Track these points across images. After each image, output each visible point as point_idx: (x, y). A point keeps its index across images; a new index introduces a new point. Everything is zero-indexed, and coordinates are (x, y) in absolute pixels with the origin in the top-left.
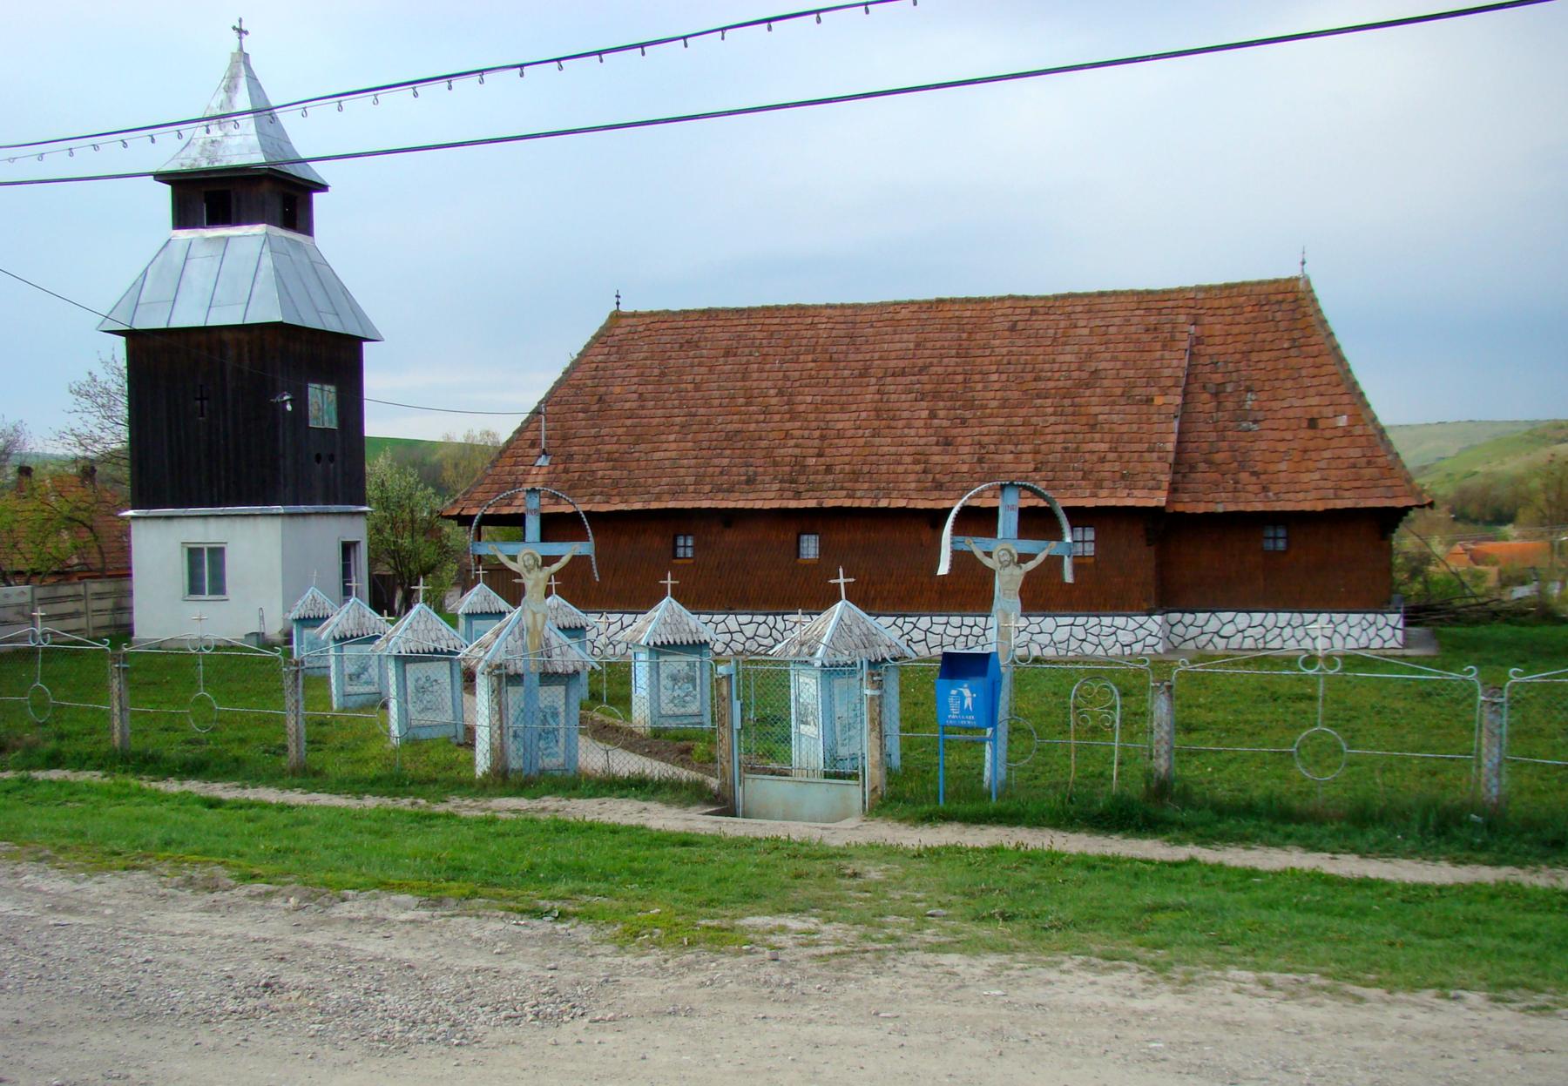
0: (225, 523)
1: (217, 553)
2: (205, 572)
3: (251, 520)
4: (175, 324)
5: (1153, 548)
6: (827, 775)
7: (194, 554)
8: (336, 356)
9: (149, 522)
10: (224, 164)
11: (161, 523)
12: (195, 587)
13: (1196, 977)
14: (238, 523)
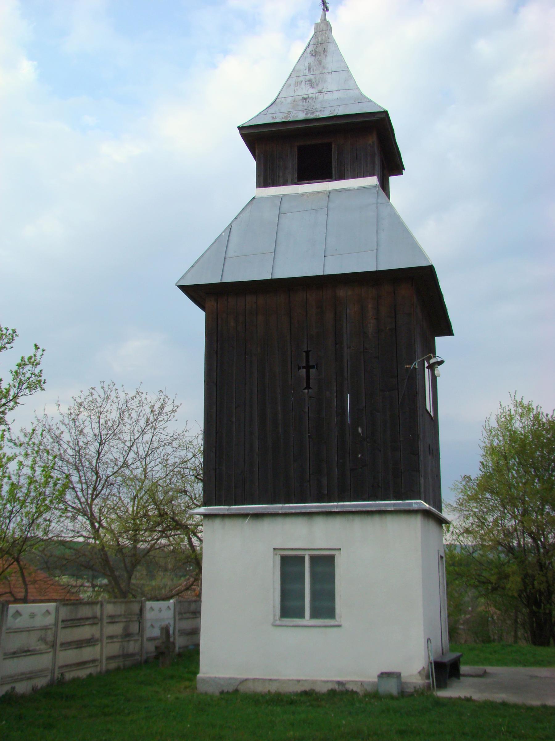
0: (337, 523)
1: (324, 564)
2: (307, 589)
3: (377, 519)
4: (278, 275)
5: (217, 693)
6: (340, 549)
7: (290, 564)
9: (229, 523)
10: (326, 114)
11: (247, 525)
12: (289, 608)
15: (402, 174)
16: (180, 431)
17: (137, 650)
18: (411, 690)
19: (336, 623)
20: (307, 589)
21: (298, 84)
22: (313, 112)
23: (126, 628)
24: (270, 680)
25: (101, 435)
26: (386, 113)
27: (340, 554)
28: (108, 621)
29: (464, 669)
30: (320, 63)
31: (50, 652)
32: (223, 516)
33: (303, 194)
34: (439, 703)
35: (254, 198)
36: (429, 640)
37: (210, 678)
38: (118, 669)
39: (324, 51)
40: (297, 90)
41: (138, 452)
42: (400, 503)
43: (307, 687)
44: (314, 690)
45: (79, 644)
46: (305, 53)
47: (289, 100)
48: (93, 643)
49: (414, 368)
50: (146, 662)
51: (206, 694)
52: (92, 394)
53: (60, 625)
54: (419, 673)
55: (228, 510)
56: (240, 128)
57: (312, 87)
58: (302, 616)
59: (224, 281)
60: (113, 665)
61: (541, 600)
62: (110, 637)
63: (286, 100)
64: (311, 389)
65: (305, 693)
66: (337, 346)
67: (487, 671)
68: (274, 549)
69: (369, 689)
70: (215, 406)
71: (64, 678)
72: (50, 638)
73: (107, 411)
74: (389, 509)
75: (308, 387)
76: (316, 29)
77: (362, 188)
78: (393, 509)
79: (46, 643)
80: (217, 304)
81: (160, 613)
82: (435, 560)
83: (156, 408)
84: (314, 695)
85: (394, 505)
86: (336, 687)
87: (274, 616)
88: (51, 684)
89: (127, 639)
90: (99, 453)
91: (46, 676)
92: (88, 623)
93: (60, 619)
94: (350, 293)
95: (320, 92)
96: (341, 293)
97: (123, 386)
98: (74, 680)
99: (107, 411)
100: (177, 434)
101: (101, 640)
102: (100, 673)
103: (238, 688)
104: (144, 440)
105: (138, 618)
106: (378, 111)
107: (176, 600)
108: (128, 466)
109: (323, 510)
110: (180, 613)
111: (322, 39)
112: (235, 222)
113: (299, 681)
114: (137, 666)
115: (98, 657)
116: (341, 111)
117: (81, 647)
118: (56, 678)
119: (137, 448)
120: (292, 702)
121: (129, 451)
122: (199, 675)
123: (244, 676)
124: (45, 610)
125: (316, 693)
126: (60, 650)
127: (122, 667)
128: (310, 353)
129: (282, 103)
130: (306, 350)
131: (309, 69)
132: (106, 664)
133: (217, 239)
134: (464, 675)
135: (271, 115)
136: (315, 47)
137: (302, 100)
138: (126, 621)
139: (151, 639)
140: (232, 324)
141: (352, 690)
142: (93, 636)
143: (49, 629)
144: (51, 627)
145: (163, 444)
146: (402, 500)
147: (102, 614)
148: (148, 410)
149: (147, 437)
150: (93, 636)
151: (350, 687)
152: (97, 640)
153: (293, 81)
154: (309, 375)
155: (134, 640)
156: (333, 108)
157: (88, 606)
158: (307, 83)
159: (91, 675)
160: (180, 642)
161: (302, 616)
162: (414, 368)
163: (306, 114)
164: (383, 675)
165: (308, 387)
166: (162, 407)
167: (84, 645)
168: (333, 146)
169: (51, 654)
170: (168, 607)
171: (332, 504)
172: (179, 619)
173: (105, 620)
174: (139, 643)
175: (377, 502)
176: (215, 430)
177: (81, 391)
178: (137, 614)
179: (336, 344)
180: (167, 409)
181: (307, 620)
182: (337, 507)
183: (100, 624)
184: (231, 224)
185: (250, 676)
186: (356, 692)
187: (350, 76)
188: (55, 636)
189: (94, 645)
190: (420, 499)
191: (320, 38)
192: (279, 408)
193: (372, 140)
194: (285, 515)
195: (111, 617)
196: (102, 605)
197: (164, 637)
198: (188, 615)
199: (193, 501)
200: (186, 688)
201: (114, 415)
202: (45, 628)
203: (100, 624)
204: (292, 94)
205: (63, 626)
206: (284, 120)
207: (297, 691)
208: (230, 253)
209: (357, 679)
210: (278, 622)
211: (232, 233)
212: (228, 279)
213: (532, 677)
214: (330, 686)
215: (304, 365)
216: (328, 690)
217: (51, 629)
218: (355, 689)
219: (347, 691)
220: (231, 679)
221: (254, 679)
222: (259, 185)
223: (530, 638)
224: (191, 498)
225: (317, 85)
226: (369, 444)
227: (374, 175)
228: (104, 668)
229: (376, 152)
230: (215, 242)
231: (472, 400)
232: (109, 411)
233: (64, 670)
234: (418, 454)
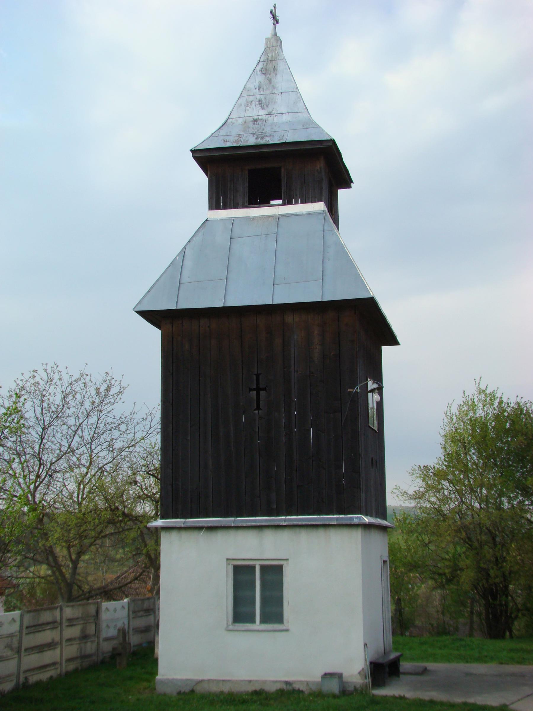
0: (285, 535)
1: (273, 573)
2: (257, 594)
3: (321, 532)
5: (175, 694)
6: (288, 559)
7: (242, 573)
8: (359, 329)
9: (185, 535)
10: (275, 140)
12: (241, 614)
16: (127, 414)
18: (352, 688)
19: (284, 628)
20: (257, 594)
21: (249, 104)
22: (263, 137)
23: (83, 630)
24: (224, 681)
25: (44, 420)
26: (333, 141)
27: (288, 564)
28: (67, 624)
29: (405, 665)
30: (270, 82)
32: (180, 529)
33: (254, 218)
34: (375, 701)
35: (206, 220)
36: (365, 645)
38: (76, 671)
39: (274, 69)
40: (248, 110)
41: (82, 436)
42: (343, 517)
43: (257, 687)
44: (264, 690)
45: (41, 648)
46: (255, 71)
47: (240, 121)
49: (356, 392)
50: (103, 662)
51: (165, 694)
52: (34, 377)
53: (25, 631)
54: (359, 673)
55: (184, 523)
56: (193, 151)
58: (253, 621)
59: (179, 307)
60: (72, 667)
62: (69, 640)
63: (237, 121)
64: (261, 410)
65: (257, 693)
66: (285, 370)
68: (227, 559)
69: (314, 688)
70: (171, 425)
72: (15, 644)
73: (50, 394)
74: (333, 523)
75: (258, 408)
77: (310, 214)
78: (336, 523)
79: (12, 649)
81: (115, 613)
82: (378, 564)
83: (102, 390)
85: (337, 519)
87: (228, 621)
88: (16, 689)
89: (84, 641)
90: (42, 438)
91: (13, 680)
92: (49, 627)
93: (25, 625)
95: (270, 114)
97: (66, 368)
98: (38, 683)
99: (50, 394)
100: (124, 417)
101: (61, 643)
103: (195, 689)
104: (90, 423)
105: (95, 619)
106: (325, 139)
107: (130, 599)
108: (73, 451)
109: (272, 523)
110: (134, 612)
111: (272, 57)
112: (188, 246)
113: (250, 681)
114: (94, 667)
115: (58, 660)
116: (291, 137)
118: (21, 682)
119: (82, 431)
120: (244, 702)
121: (74, 435)
122: (158, 677)
123: (201, 678)
125: (266, 693)
126: (25, 655)
127: (80, 668)
128: (260, 376)
130: (256, 373)
131: (260, 88)
132: (66, 666)
133: (171, 263)
134: (404, 673)
135: (222, 138)
136: (265, 64)
137: (253, 121)
138: (83, 624)
139: (107, 639)
141: (299, 689)
142: (53, 640)
143: (14, 636)
145: (109, 428)
147: (61, 618)
148: (93, 393)
149: (93, 420)
150: (53, 640)
151: (297, 686)
152: (57, 644)
153: (243, 100)
154: (259, 396)
155: (91, 641)
157: (48, 612)
158: (257, 103)
159: (51, 677)
160: (134, 640)
161: (253, 621)
162: (356, 392)
163: (256, 139)
164: (327, 676)
165: (258, 408)
166: (108, 389)
167: (45, 649)
168: (283, 170)
169: (16, 660)
171: (281, 517)
172: (134, 618)
173: (65, 623)
174: (95, 644)
175: (322, 516)
177: (23, 374)
178: (94, 616)
179: (284, 368)
180: (114, 390)
181: (258, 625)
182: (285, 520)
184: (184, 248)
185: (206, 677)
186: (302, 692)
187: (300, 97)
188: (20, 642)
189: (55, 648)
190: (361, 514)
191: (270, 55)
193: (320, 165)
194: (237, 528)
195: (69, 620)
196: (61, 610)
197: (121, 638)
198: (141, 613)
199: (143, 492)
200: (145, 689)
201: (58, 400)
202: (11, 636)
203: (59, 628)
204: (242, 115)
206: (235, 145)
207: (248, 691)
208: (185, 279)
210: (231, 627)
211: (186, 257)
213: (468, 674)
214: (278, 686)
216: (277, 690)
217: (16, 636)
218: (301, 689)
220: (187, 680)
222: (211, 208)
224: (141, 488)
225: (267, 106)
227: (321, 201)
228: (64, 671)
229: (324, 177)
230: (170, 266)
231: (418, 406)
232: (52, 394)
233: (28, 674)
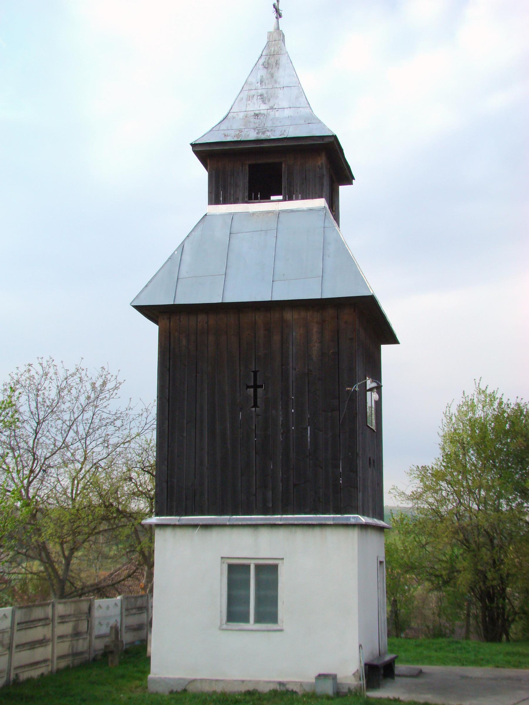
0: (280, 534)
1: (268, 572)
2: (251, 594)
3: (317, 532)
5: (167, 693)
6: (283, 559)
7: (236, 572)
8: (359, 327)
9: (179, 532)
12: (235, 613)
13: (82, 618)
14: (300, 535)
15: (351, 183)
16: (123, 409)
17: (85, 648)
18: (345, 690)
19: (279, 628)
20: (251, 594)
21: (250, 98)
22: (264, 132)
23: (75, 627)
25: (38, 415)
26: (335, 137)
27: (283, 563)
28: (59, 621)
29: (400, 667)
30: (272, 76)
31: (6, 654)
33: (253, 214)
35: (206, 215)
36: (360, 646)
37: (160, 678)
38: (67, 668)
39: (276, 64)
41: (77, 431)
43: (251, 688)
44: (257, 690)
45: (32, 645)
46: (257, 65)
47: (241, 115)
48: (45, 644)
49: (355, 390)
50: (94, 660)
51: (157, 693)
53: (16, 627)
54: (354, 674)
56: (193, 145)
57: (264, 102)
60: (63, 664)
61: (494, 593)
62: (60, 637)
66: (283, 367)
67: (423, 670)
68: (222, 558)
69: (308, 689)
70: (167, 422)
71: (18, 678)
72: (6, 641)
73: (45, 388)
74: (329, 523)
75: (255, 405)
76: (269, 38)
77: (311, 210)
78: (332, 523)
80: (170, 322)
81: (108, 610)
83: (98, 385)
84: (257, 695)
85: (334, 519)
86: (278, 687)
87: (221, 620)
92: (40, 624)
94: (296, 316)
95: (272, 108)
96: (289, 315)
97: (62, 362)
98: (29, 680)
99: (45, 388)
101: (53, 640)
102: (51, 672)
103: (187, 688)
107: (123, 597)
108: (67, 447)
110: (127, 610)
112: (187, 240)
113: (243, 681)
114: (86, 665)
115: (50, 657)
116: (292, 133)
117: (34, 648)
119: (77, 426)
121: (69, 430)
122: (151, 676)
124: (3, 614)
125: (259, 693)
127: (71, 665)
128: (258, 374)
129: (234, 118)
130: (254, 370)
131: (261, 82)
132: (57, 663)
133: (170, 258)
134: (399, 676)
135: (223, 132)
136: (267, 59)
137: (254, 116)
138: (76, 621)
139: (99, 637)
140: (184, 342)
142: (45, 636)
144: (7, 630)
145: (104, 423)
146: (341, 514)
148: (89, 387)
149: (88, 415)
150: (45, 636)
151: (290, 687)
152: (48, 641)
153: (244, 95)
156: (284, 128)
157: (40, 608)
158: (259, 97)
159: (42, 674)
160: (127, 638)
162: (355, 390)
163: (257, 133)
164: (321, 677)
165: (255, 405)
166: (104, 384)
167: (36, 646)
168: (283, 166)
170: (116, 604)
171: (276, 516)
172: (126, 616)
173: (57, 620)
175: (318, 516)
176: (167, 444)
177: (18, 368)
178: (86, 613)
181: (252, 624)
182: (281, 519)
183: (51, 625)
185: (198, 677)
188: (11, 638)
189: (46, 645)
190: (358, 514)
191: (272, 49)
192: (228, 425)
193: (322, 161)
194: (232, 526)
195: (61, 617)
196: (53, 606)
197: (113, 636)
198: (134, 611)
200: (137, 687)
201: (53, 394)
203: (51, 625)
205: (18, 628)
207: (241, 691)
209: (297, 680)
210: (225, 626)
211: (184, 252)
212: (181, 301)
213: (463, 677)
214: (272, 687)
215: (252, 384)
216: (270, 691)
218: (294, 690)
219: (287, 691)
221: (201, 680)
222: (211, 202)
223: (482, 633)
225: (269, 100)
226: (311, 461)
227: (322, 197)
228: (55, 668)
229: (325, 173)
230: (168, 260)
232: (47, 388)
233: (18, 671)
234: (357, 472)
